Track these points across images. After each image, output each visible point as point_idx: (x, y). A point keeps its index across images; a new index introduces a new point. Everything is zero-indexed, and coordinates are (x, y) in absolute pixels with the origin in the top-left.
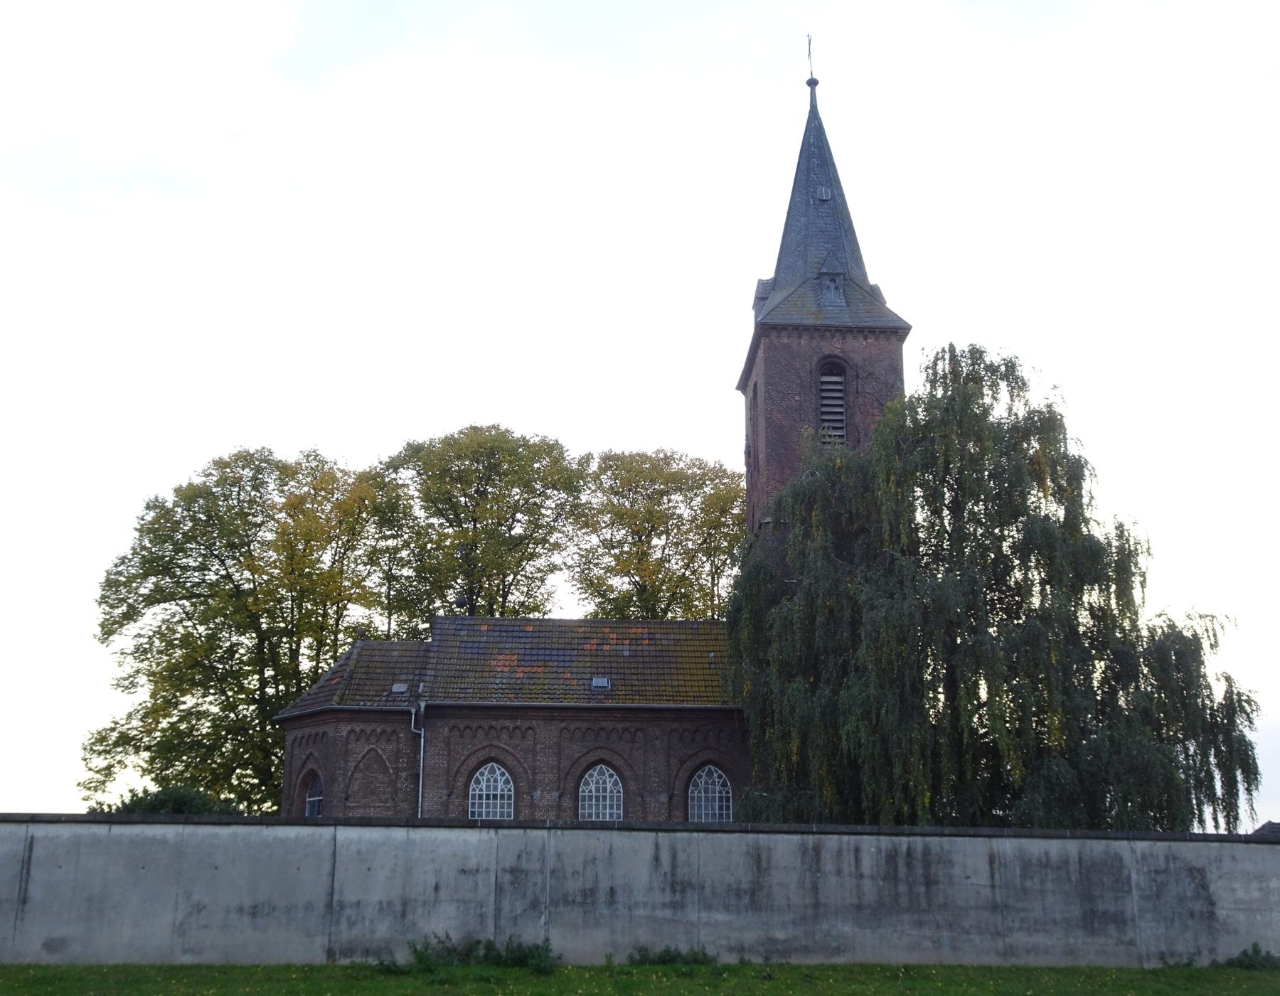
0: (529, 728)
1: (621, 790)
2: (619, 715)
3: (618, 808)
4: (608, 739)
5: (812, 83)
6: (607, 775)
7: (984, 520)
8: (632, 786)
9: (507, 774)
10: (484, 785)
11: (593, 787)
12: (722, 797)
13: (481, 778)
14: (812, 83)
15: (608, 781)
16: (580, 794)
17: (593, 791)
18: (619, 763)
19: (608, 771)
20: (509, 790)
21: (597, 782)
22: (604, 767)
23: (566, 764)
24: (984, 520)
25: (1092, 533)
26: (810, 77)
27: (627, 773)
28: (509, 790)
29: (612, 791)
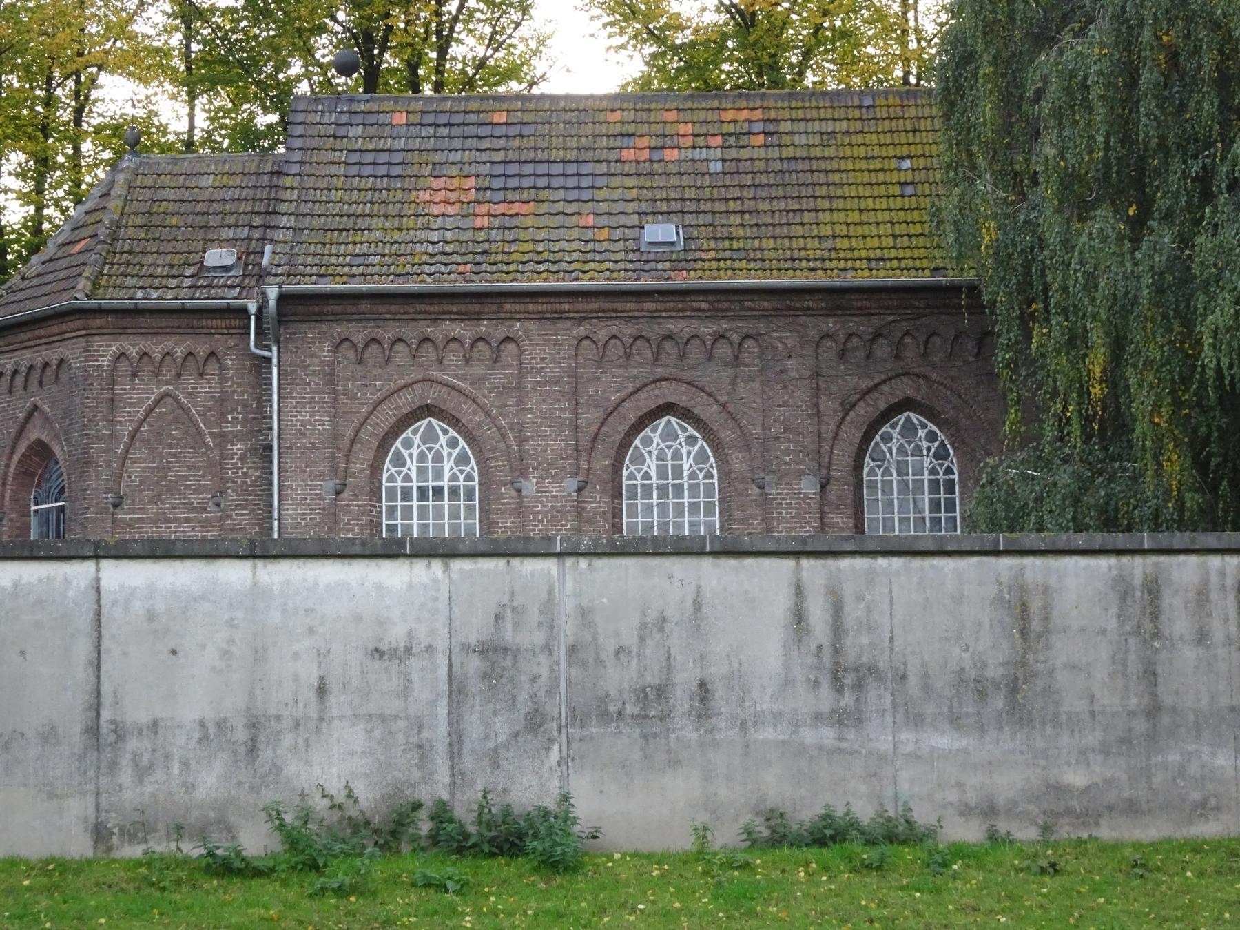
0: (507, 339)
1: (715, 472)
8: (738, 462)
11: (652, 466)
13: (405, 453)
15: (684, 451)
18: (706, 410)
19: (444, 434)
23: (590, 416)
27: (726, 435)
29: (693, 475)
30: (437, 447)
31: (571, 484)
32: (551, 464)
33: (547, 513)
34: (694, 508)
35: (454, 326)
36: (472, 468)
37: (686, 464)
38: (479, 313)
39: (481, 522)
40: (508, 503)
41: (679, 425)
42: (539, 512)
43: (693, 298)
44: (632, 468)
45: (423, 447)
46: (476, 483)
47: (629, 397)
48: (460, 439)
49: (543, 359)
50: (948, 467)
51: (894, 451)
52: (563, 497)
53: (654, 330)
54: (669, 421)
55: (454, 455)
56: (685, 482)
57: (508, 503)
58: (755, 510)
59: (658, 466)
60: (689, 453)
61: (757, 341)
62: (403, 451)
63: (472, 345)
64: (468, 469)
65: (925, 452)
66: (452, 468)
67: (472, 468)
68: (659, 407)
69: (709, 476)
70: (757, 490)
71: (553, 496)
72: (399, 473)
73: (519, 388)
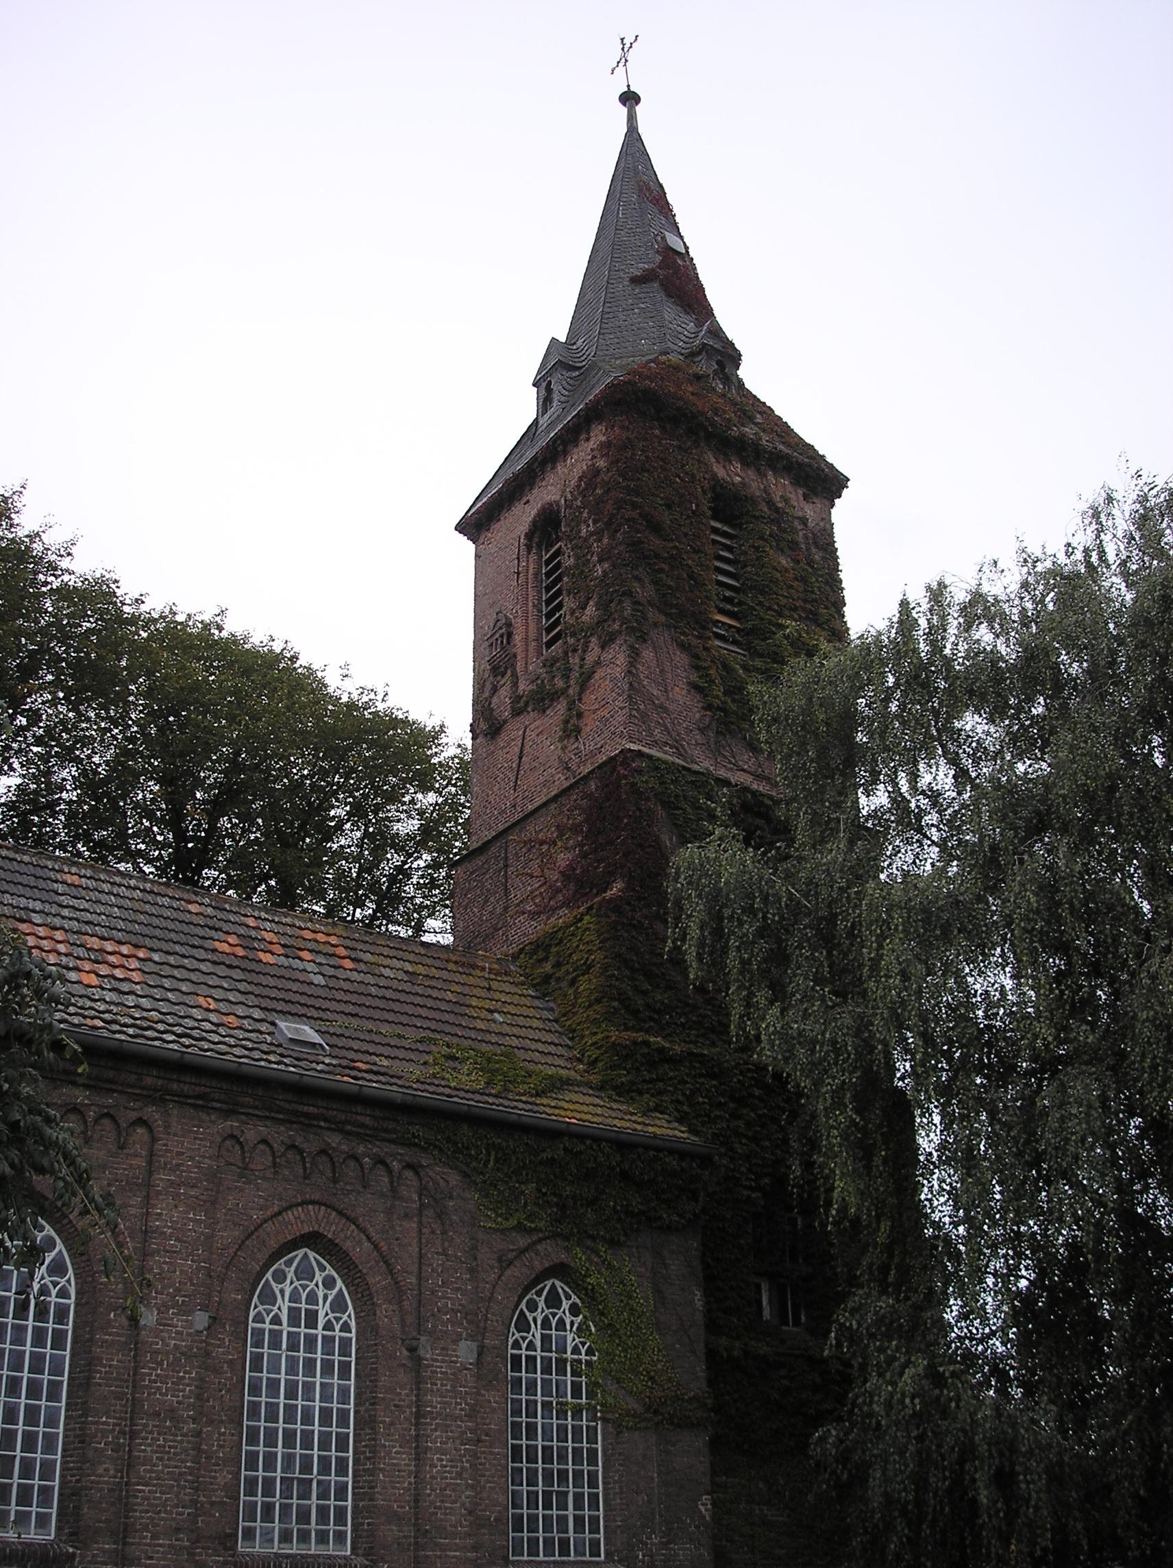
0: (141, 1122)
1: (353, 1324)
2: (367, 1120)
3: (344, 1374)
4: (335, 1181)
5: (630, 99)
6: (319, 1277)
7: (1039, 1238)
8: (385, 1314)
9: (339, 1283)
10: (536, 1333)
11: (283, 1306)
12: (580, 1361)
13: (276, 1287)
14: (630, 99)
15: (320, 1294)
16: (251, 1325)
17: (284, 1318)
18: (359, 1250)
19: (322, 1270)
20: (63, 1294)
21: (295, 1297)
22: (311, 1254)
23: (227, 1236)
24: (1039, 1238)
25: (632, 89)
26: (626, 89)
27: (378, 1280)
28: (63, 1294)
29: (328, 1326)
30: (312, 1285)
31: (201, 1320)
32: (178, 1290)
33: (168, 1353)
34: (328, 1368)
35: (77, 1092)
36: (349, 1316)
37: (323, 1311)
38: (111, 1081)
39: (73, 1355)
40: (118, 1335)
41: (315, 1259)
42: (157, 1352)
43: (359, 1109)
44: (261, 1308)
45: (296, 1283)
46: (353, 1335)
47: (272, 1217)
48: (58, 1241)
49: (180, 1154)
50: (276, 1316)
51: (539, 1322)
52: (189, 1334)
53: (311, 1145)
54: (306, 1255)
55: (330, 1298)
56: (319, 1331)
57: (118, 1335)
58: (402, 1376)
59: (290, 1308)
60: (325, 1297)
61: (417, 1173)
62: (274, 1284)
63: (96, 1121)
64: (63, 1281)
65: (568, 1327)
66: (327, 1314)
67: (69, 1281)
68: (302, 1236)
69: (346, 1328)
70: (406, 1353)
71: (177, 1333)
72: (55, 1284)
73: (148, 1184)
